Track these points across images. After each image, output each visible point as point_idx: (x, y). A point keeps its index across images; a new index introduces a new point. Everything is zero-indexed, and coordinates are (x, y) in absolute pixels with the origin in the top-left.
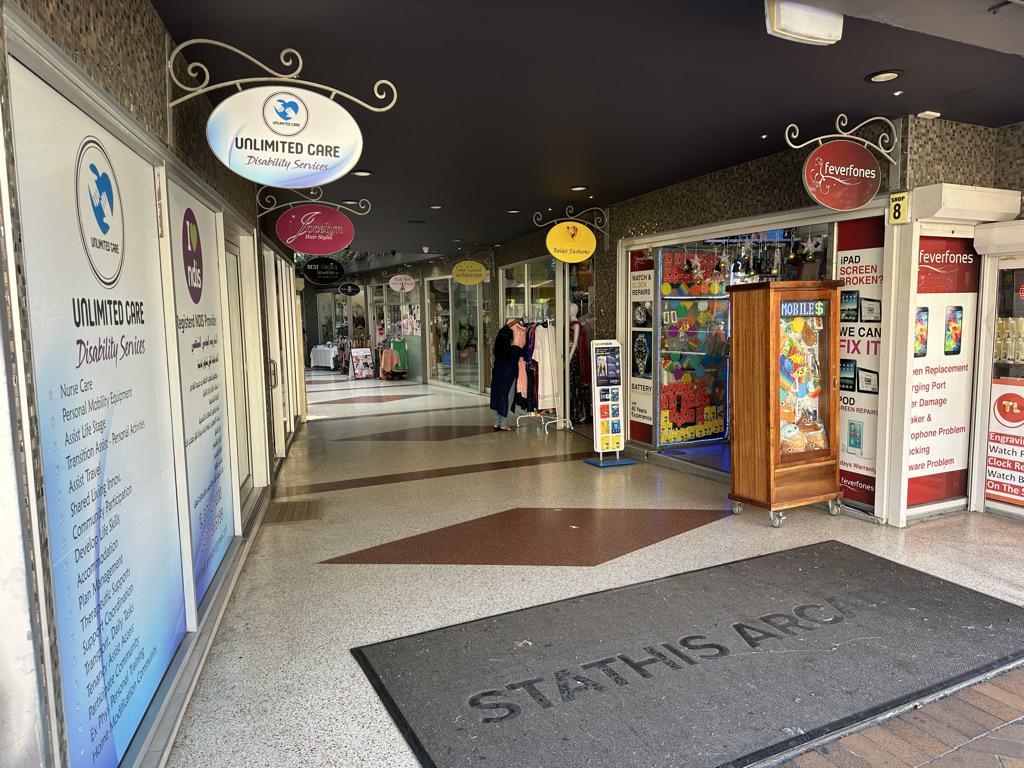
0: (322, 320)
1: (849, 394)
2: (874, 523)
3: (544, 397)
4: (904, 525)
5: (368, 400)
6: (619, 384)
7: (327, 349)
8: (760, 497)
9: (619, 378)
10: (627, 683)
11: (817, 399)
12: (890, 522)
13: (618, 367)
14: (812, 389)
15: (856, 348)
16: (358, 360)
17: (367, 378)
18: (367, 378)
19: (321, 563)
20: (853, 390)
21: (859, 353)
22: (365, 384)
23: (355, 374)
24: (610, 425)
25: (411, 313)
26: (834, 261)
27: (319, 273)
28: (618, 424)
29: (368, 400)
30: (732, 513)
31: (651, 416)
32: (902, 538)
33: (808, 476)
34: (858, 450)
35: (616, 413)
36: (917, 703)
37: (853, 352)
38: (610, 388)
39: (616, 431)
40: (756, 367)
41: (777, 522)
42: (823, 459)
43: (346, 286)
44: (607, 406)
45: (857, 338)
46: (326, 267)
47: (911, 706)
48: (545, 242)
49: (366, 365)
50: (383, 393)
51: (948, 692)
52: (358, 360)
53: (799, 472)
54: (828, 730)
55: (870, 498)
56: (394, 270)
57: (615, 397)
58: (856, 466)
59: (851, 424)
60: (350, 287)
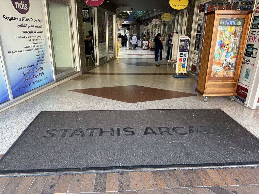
0: (141, 33)
1: (248, 58)
2: (244, 106)
3: (174, 56)
4: (255, 108)
5: (146, 55)
6: (187, 52)
7: (140, 41)
8: (202, 91)
9: (187, 50)
10: (69, 137)
11: (235, 59)
12: (249, 107)
13: (188, 46)
14: (233, 55)
15: (255, 40)
16: (144, 44)
17: (146, 49)
18: (146, 49)
19: (68, 90)
20: (250, 57)
21: (255, 42)
22: (145, 51)
23: (143, 48)
24: (182, 65)
25: (158, 31)
26: (255, 3)
27: (123, 16)
28: (185, 65)
29: (146, 55)
30: (196, 95)
31: (196, 63)
32: (252, 113)
33: (224, 86)
34: (247, 79)
35: (184, 61)
36: (176, 169)
37: (253, 42)
38: (183, 53)
39: (183, 67)
40: (208, 44)
41: (205, 100)
42: (230, 81)
43: (145, 23)
44: (182, 58)
45: (255, 36)
46: (125, 15)
47: (173, 169)
48: (169, 4)
49: (146, 46)
50: (149, 53)
51: (194, 168)
52: (144, 44)
53: (218, 84)
54: (131, 167)
55: (245, 96)
56: (153, 18)
57: (185, 56)
58: (245, 85)
59: (247, 69)
60: (146, 23)
